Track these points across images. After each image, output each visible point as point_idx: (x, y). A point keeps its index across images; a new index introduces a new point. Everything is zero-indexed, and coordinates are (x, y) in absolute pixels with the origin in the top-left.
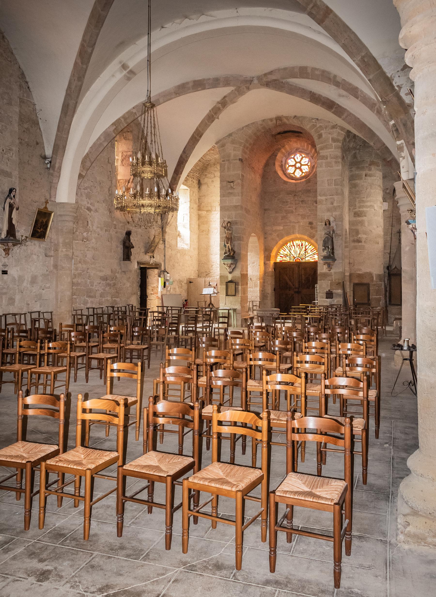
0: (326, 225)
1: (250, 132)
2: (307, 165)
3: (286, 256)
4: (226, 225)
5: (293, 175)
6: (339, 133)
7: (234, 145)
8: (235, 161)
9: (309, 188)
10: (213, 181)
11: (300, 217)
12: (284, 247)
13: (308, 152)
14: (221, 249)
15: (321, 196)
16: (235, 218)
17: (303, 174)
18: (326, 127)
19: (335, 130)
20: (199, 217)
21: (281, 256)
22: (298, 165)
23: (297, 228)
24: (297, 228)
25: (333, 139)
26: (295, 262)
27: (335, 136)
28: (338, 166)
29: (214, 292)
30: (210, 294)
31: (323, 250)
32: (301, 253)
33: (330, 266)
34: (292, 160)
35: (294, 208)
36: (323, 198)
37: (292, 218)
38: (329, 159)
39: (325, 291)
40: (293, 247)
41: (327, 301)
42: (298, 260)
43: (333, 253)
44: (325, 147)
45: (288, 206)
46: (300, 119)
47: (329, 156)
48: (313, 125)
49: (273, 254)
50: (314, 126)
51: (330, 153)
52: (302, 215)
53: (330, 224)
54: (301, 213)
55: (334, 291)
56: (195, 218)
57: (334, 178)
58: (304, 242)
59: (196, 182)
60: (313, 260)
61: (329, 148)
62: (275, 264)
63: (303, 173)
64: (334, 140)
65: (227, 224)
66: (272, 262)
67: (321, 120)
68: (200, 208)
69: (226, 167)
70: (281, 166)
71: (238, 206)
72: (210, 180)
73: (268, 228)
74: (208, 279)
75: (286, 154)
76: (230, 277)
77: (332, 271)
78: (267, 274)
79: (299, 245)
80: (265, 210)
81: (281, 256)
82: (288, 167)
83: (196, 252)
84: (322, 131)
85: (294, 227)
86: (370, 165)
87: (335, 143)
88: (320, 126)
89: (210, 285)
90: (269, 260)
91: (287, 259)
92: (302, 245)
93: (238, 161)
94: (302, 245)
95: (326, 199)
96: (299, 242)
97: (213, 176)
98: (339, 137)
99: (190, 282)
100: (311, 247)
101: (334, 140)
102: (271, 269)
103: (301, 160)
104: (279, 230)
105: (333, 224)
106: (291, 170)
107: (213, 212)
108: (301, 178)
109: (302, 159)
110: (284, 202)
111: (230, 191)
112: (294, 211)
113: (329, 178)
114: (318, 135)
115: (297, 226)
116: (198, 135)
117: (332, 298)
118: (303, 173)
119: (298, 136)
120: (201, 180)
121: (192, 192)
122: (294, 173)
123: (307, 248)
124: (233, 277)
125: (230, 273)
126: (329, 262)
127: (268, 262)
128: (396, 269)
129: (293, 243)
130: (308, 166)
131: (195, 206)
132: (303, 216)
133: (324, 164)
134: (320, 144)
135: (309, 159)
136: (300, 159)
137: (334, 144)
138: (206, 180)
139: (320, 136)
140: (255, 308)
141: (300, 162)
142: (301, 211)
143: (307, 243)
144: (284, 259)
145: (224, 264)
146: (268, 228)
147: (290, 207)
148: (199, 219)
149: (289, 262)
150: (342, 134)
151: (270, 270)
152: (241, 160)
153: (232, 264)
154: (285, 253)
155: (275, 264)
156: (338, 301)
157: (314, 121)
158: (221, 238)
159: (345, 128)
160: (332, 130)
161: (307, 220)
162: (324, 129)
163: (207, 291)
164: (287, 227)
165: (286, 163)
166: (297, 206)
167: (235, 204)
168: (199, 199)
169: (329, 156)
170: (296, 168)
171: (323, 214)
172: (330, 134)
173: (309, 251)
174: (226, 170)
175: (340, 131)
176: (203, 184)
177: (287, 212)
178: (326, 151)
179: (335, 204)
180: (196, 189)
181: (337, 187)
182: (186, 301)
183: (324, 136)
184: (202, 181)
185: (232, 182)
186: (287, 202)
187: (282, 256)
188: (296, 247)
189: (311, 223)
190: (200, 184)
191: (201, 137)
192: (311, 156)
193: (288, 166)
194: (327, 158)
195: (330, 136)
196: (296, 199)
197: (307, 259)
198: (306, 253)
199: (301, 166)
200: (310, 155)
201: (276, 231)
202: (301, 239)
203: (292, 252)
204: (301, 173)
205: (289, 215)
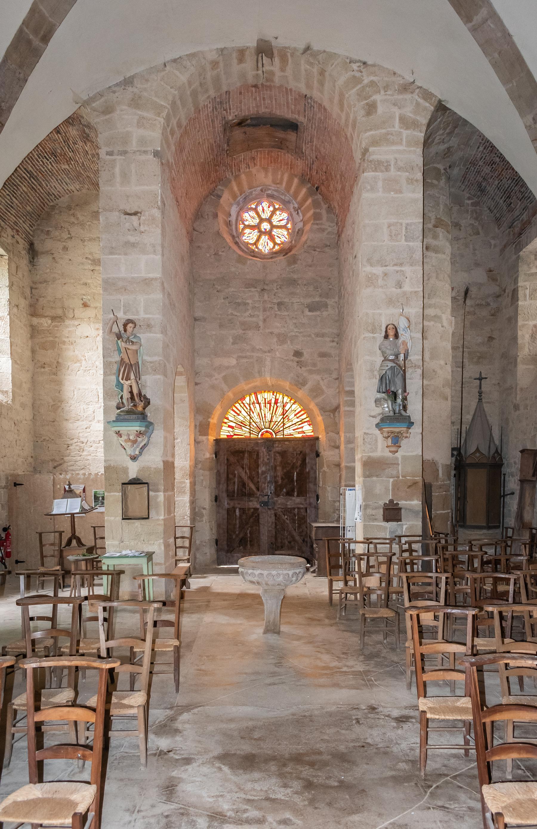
0: (386, 337)
1: (183, 78)
2: (284, 227)
3: (241, 425)
4: (122, 329)
5: (254, 247)
6: (418, 104)
7: (139, 112)
8: (143, 157)
9: (295, 276)
10: (65, 249)
11: (275, 340)
12: (237, 405)
13: (287, 199)
14: (107, 395)
15: (371, 266)
16: (146, 312)
17: (277, 247)
18: (386, 88)
19: (408, 96)
20: (34, 332)
21: (229, 426)
22: (265, 226)
23: (268, 363)
24: (268, 363)
25: (403, 119)
26: (262, 439)
27: (408, 111)
28: (413, 192)
29: (82, 507)
30: (73, 515)
31: (377, 401)
32: (274, 419)
33: (396, 440)
34: (252, 213)
35: (261, 318)
36: (378, 270)
37: (256, 339)
38: (393, 172)
39: (381, 503)
40: (257, 405)
41: (385, 528)
42: (268, 435)
43: (405, 408)
44: (383, 140)
45: (247, 314)
46: (320, 57)
47: (392, 163)
48: (354, 77)
49: (214, 420)
50: (356, 81)
51: (397, 156)
52: (279, 335)
53: (396, 336)
54: (276, 331)
55: (402, 503)
56: (24, 333)
57: (405, 221)
58: (280, 397)
59: (22, 245)
60: (300, 435)
61: (393, 143)
62: (218, 441)
63: (275, 244)
64: (405, 122)
65: (125, 326)
66: (212, 438)
67: (374, 65)
68: (34, 310)
69: (117, 170)
70: (228, 224)
71: (152, 279)
72: (60, 245)
73: (202, 362)
74: (62, 477)
75: (240, 198)
76: (133, 470)
77: (399, 455)
78: (200, 466)
79: (270, 403)
80: (196, 320)
81: (229, 426)
82: (243, 229)
83: (27, 414)
84: (377, 97)
85: (260, 361)
86: (435, 226)
87: (409, 132)
88: (372, 83)
89: (71, 491)
90: (206, 434)
91: (243, 433)
92: (276, 402)
93: (152, 157)
94: (276, 402)
95: (386, 274)
96: (269, 396)
97: (65, 235)
98: (418, 118)
99: (16, 485)
100: (297, 407)
101: (405, 122)
102: (208, 454)
103: (271, 216)
104: (228, 368)
105: (404, 336)
106: (250, 237)
107: (67, 322)
108: (273, 254)
109: (273, 213)
110: (239, 304)
111: (132, 239)
112: (261, 324)
113: (393, 220)
114: (367, 104)
115: (269, 359)
116: (36, 32)
117: (400, 520)
118: (275, 244)
119: (281, 145)
120: (36, 243)
121: (13, 265)
122: (256, 244)
123: (287, 408)
124: (142, 470)
125: (134, 458)
126: (397, 430)
127: (204, 438)
128: (478, 455)
129: (257, 398)
130: (288, 229)
131: (23, 303)
132: (282, 338)
133: (380, 184)
134: (371, 130)
135: (290, 215)
136: (269, 214)
137: (405, 133)
138: (49, 244)
139: (371, 108)
140: (179, 542)
141: (269, 220)
142: (277, 327)
143: (286, 399)
144: (237, 431)
145: (118, 433)
146: (202, 362)
147: (251, 316)
148: (32, 337)
149: (250, 439)
150: (425, 109)
151: (208, 455)
152: (156, 154)
153: (140, 434)
154: (241, 418)
155: (218, 441)
156: (411, 525)
157: (355, 66)
158: (107, 365)
159: (432, 94)
160: (401, 97)
161: (290, 347)
162: (382, 92)
163: (62, 506)
164: (245, 360)
165: (239, 218)
166: (268, 313)
167: (143, 275)
168: (32, 288)
169: (392, 163)
170: (261, 233)
171: (378, 311)
172: (395, 104)
173: (292, 416)
174: (118, 179)
175: (421, 101)
176: (43, 253)
177: (246, 326)
178: (384, 148)
179: (407, 288)
180: (24, 263)
181: (411, 244)
182: (5, 529)
183: (381, 109)
184: (38, 246)
185: (135, 214)
186: (246, 304)
187: (233, 425)
188: (262, 405)
189: (298, 354)
190: (33, 252)
191: (46, 39)
192: (294, 208)
193: (242, 226)
194: (387, 169)
195: (397, 112)
196: (266, 297)
197: (286, 432)
198: (286, 420)
199: (271, 230)
200: (291, 206)
201: (219, 369)
202: (274, 389)
203: (255, 416)
204: (271, 245)
205: (250, 333)
